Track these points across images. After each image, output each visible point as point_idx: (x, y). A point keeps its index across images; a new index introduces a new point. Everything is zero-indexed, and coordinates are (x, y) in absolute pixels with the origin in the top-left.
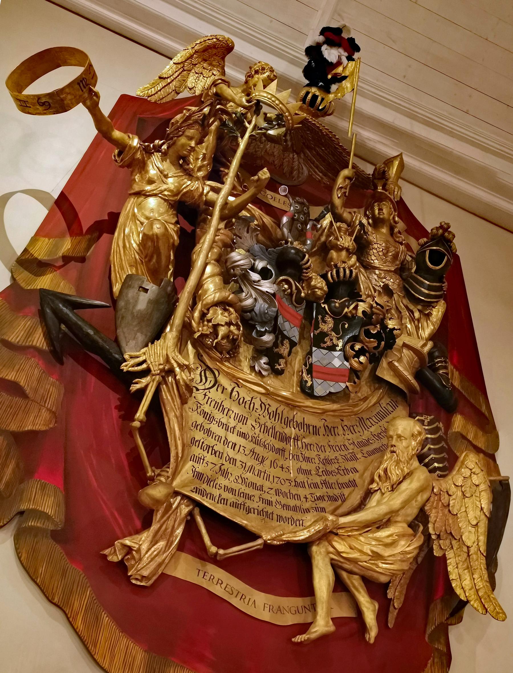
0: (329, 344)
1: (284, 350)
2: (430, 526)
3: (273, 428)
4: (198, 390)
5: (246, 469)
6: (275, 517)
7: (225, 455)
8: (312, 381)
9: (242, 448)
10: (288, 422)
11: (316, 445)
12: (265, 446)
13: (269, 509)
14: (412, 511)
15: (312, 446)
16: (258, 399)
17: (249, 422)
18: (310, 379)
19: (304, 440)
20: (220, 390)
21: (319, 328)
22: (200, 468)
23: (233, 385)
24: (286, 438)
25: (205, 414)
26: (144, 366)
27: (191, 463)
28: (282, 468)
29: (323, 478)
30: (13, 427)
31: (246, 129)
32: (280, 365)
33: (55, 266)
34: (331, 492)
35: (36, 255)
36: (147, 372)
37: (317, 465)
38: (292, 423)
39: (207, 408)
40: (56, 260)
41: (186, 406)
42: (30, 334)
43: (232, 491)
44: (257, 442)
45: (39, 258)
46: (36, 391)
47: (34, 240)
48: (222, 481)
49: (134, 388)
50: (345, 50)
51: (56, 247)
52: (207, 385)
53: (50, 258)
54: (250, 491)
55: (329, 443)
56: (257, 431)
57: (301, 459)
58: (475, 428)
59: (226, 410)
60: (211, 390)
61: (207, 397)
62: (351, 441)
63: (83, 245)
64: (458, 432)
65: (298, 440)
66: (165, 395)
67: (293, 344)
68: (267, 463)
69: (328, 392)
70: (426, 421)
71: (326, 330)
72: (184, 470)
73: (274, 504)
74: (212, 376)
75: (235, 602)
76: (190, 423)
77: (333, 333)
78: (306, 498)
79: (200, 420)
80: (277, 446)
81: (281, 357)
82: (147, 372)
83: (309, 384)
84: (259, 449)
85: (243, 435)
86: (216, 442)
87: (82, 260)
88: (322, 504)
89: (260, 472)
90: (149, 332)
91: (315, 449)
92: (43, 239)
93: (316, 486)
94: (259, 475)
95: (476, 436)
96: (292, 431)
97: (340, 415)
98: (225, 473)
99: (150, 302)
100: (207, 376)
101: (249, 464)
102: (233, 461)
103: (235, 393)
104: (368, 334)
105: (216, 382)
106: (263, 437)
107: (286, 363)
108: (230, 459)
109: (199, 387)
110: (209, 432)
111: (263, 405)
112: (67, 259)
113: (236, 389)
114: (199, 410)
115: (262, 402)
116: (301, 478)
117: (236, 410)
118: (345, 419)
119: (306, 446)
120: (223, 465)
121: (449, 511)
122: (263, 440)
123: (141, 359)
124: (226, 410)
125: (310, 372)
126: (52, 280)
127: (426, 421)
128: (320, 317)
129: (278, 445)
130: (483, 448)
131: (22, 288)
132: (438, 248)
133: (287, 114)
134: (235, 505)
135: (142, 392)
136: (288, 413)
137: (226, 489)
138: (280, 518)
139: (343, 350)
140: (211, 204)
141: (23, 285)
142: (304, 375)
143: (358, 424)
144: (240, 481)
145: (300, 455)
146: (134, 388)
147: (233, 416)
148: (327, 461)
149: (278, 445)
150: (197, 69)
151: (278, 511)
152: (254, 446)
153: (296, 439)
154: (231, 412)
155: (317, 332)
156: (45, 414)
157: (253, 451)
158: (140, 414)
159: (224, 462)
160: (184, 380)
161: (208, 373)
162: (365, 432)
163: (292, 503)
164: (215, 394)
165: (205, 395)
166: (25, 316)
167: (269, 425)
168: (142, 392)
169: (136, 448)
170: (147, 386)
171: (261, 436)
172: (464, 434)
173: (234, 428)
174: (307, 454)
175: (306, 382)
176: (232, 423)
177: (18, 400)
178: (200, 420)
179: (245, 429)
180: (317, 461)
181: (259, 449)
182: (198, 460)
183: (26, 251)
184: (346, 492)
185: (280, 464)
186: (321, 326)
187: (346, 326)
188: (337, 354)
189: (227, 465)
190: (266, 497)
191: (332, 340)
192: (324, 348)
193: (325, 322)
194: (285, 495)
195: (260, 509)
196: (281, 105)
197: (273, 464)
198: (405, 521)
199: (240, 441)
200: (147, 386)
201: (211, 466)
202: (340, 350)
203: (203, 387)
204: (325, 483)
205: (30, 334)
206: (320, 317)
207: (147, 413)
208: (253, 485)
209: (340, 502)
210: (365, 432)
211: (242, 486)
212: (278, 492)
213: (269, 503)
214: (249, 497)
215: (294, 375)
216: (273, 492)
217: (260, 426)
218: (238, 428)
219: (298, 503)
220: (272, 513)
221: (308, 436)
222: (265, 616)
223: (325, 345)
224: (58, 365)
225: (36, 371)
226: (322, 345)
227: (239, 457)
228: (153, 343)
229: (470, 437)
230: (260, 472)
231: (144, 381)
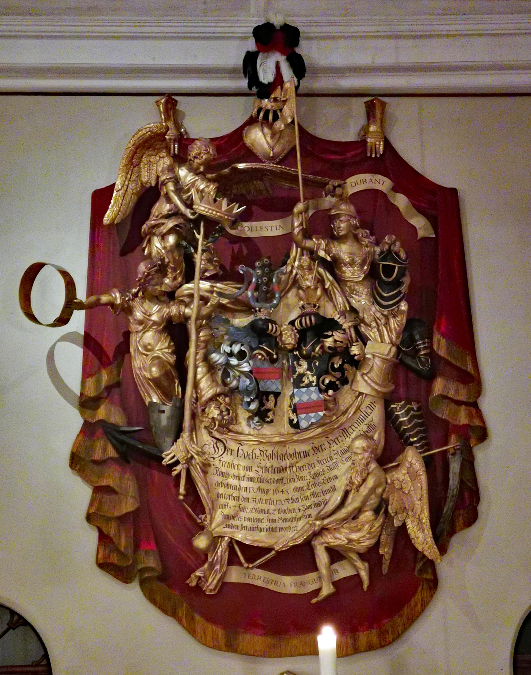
0: (307, 381)
1: (270, 404)
2: (390, 507)
3: (272, 466)
4: (214, 458)
5: (257, 502)
6: (278, 529)
7: (241, 497)
8: (297, 418)
9: (251, 489)
10: (283, 457)
11: (307, 465)
12: (267, 482)
13: (274, 525)
14: (373, 501)
15: (304, 467)
16: (258, 449)
17: (254, 469)
18: (296, 417)
19: (297, 465)
20: (229, 453)
21: (296, 372)
22: (226, 511)
23: (238, 445)
24: (283, 469)
25: (222, 474)
26: (175, 459)
27: (220, 510)
28: (282, 491)
29: (312, 490)
30: (117, 514)
31: (197, 241)
32: (269, 417)
33: (103, 398)
34: (316, 500)
35: (89, 395)
36: (177, 463)
37: (308, 480)
38: (286, 457)
39: (223, 470)
40: (101, 393)
41: (209, 475)
42: (105, 450)
43: (249, 519)
44: (261, 481)
45: (92, 396)
46: (121, 487)
47: (83, 383)
48: (242, 514)
49: (174, 473)
50: (283, 53)
51: (98, 382)
52: (221, 453)
53: (99, 392)
54: (261, 516)
55: (318, 460)
56: (260, 473)
57: (296, 480)
58: (455, 384)
59: (236, 466)
60: (223, 456)
61: (221, 462)
62: (336, 452)
63: (115, 372)
64: (438, 395)
65: (292, 467)
66: (194, 474)
67: (277, 395)
68: (271, 492)
69: (310, 423)
70: (398, 408)
71: (302, 372)
72: (216, 516)
73: (277, 520)
74: (222, 445)
75: (271, 587)
76: (214, 485)
77: (308, 372)
78: (299, 510)
79: (220, 479)
80: (276, 478)
81: (269, 410)
82: (177, 463)
83: (295, 422)
84: (263, 486)
85: (251, 479)
86: (234, 491)
87: (118, 384)
88: (308, 512)
89: (267, 500)
90: (173, 436)
91: (307, 468)
92: (88, 379)
93: (307, 498)
94: (266, 503)
95: (457, 392)
96: (287, 463)
97: (324, 434)
98: (243, 509)
99: (168, 418)
100: (218, 446)
101: (258, 498)
102: (247, 500)
103: (240, 451)
104: (334, 370)
105: (225, 448)
106: (265, 476)
107: (274, 413)
108: (244, 499)
109: (215, 456)
110: (228, 485)
111: (262, 452)
112: (109, 388)
113: (241, 447)
114: (218, 473)
115: (261, 451)
116: (297, 495)
117: (243, 463)
118: (329, 436)
119: (300, 469)
120: (240, 504)
121: (403, 492)
122: (266, 478)
123: (172, 455)
124: (236, 466)
125: (295, 411)
126: (106, 409)
127: (398, 408)
128: (295, 363)
129: (277, 476)
130: (465, 400)
131: (90, 423)
132: (382, 274)
133: (226, 217)
134: (252, 529)
135: (179, 475)
136: (280, 450)
137: (246, 519)
138: (281, 529)
139: (317, 385)
140: (187, 318)
141: (90, 420)
142: (291, 415)
143: (341, 435)
144: (254, 511)
145: (295, 477)
146: (174, 473)
147: (241, 468)
148: (317, 475)
149: (277, 476)
150: (144, 160)
151: (281, 524)
152: (260, 484)
153: (291, 466)
154: (239, 466)
155: (295, 376)
156: (131, 500)
157: (259, 489)
158: (182, 490)
159: (241, 503)
160: (200, 461)
161: (218, 444)
162: (347, 439)
163: (289, 516)
164: (227, 458)
165: (220, 460)
166: (98, 439)
167: (268, 465)
168: (179, 475)
169: (187, 510)
170: (180, 472)
171: (264, 475)
172: (445, 394)
173: (244, 476)
174: (301, 474)
175: (293, 420)
176: (242, 473)
177: (113, 497)
178: (220, 479)
179: (251, 474)
180: (308, 477)
181: (263, 486)
182: (224, 506)
183: (82, 394)
184: (327, 497)
185: (280, 490)
186: (297, 369)
187: (317, 364)
188: (312, 389)
189: (244, 504)
190: (271, 517)
191: (308, 378)
192: (303, 387)
193: (300, 365)
194: (285, 512)
195: (268, 527)
196: (218, 214)
197: (275, 491)
198: (370, 510)
199: (250, 484)
200: (180, 472)
201: (233, 508)
202: (316, 386)
203: (218, 456)
204: (314, 494)
205: (105, 450)
206: (295, 363)
207: (186, 489)
208: (263, 511)
209: (323, 506)
210: (347, 439)
211: (255, 515)
212: (279, 511)
213: (274, 521)
214: (260, 520)
215: (284, 416)
216: (276, 512)
217: (262, 468)
218: (246, 476)
219: (293, 515)
220: (276, 528)
221: (300, 460)
222: (293, 590)
223: (303, 385)
224: (127, 465)
225: (116, 474)
226: (302, 385)
227: (250, 496)
228: (176, 441)
229: (451, 394)
230: (267, 500)
231: (179, 468)
